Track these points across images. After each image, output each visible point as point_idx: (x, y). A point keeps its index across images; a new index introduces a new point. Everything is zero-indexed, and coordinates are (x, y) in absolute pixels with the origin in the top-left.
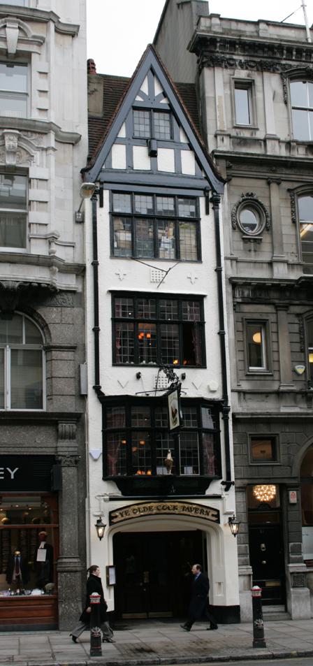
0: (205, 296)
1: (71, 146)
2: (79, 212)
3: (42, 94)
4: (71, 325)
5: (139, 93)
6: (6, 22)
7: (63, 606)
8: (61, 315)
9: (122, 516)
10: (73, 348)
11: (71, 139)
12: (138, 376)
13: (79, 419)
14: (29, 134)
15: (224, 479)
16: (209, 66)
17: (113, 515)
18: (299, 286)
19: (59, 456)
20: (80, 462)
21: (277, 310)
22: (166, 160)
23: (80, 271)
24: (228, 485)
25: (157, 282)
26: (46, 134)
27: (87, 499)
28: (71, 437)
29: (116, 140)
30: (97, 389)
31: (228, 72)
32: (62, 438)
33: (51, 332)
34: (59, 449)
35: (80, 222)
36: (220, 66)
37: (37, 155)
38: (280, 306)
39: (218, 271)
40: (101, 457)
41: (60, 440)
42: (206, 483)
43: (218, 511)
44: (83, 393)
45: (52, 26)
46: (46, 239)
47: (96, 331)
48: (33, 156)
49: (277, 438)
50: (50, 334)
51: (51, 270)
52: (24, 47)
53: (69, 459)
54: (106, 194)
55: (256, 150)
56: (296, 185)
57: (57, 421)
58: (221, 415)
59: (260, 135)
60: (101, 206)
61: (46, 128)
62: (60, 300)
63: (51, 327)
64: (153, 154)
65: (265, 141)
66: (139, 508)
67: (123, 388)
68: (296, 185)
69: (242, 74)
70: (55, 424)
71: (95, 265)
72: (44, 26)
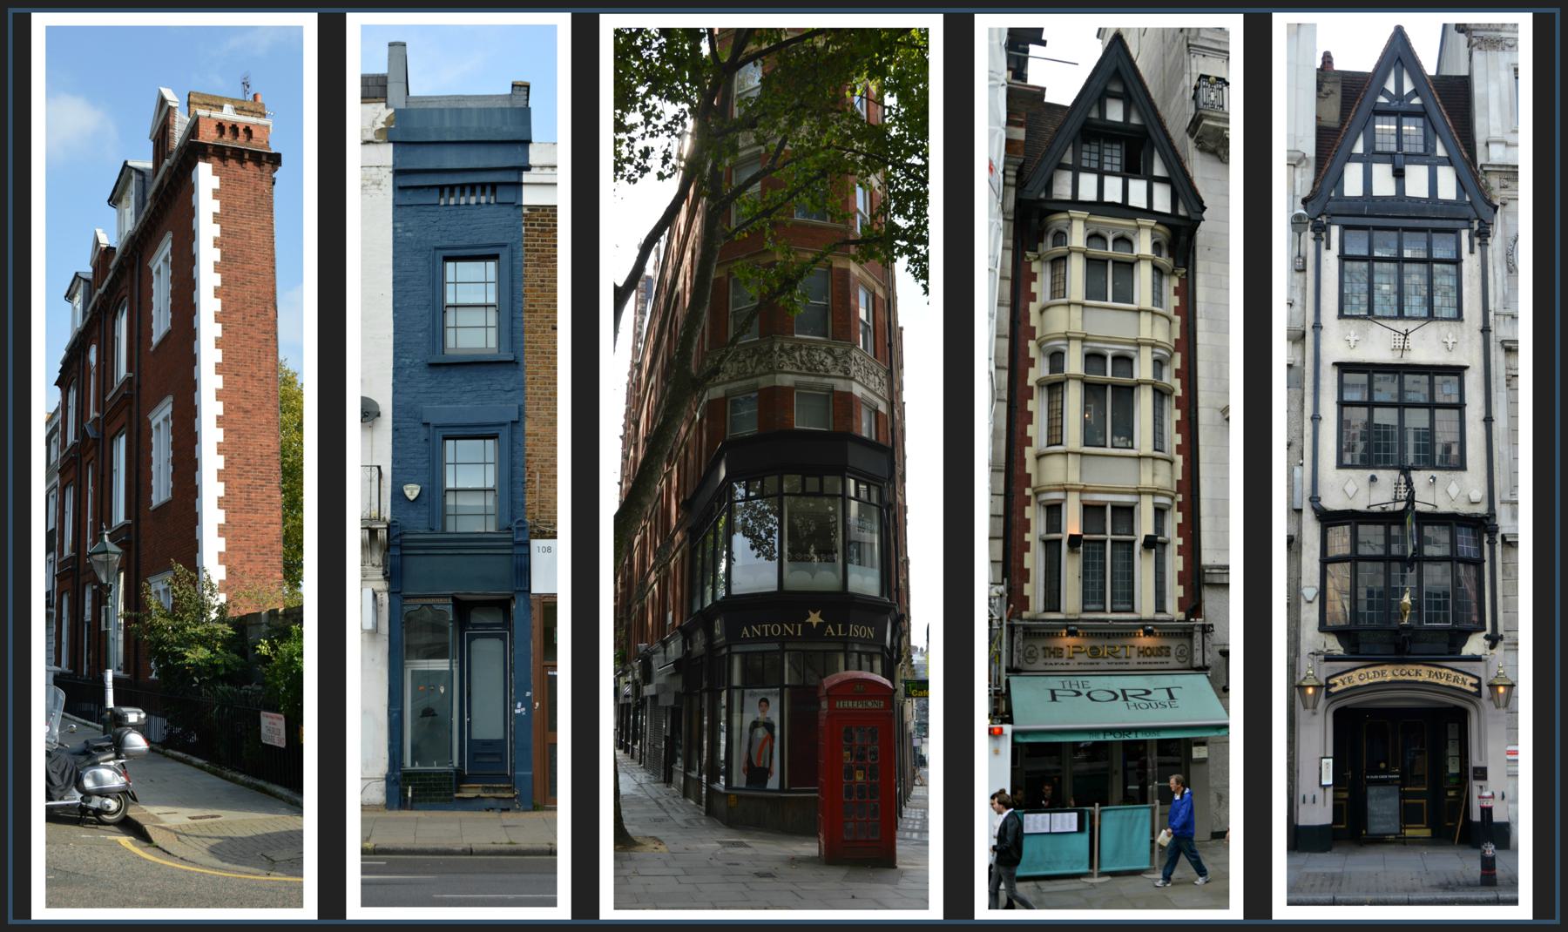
15: (1489, 631)
17: (1331, 682)
30: (1315, 499)
42: (1462, 636)
43: (1479, 679)
58: (1486, 539)
60: (1328, 248)
64: (1399, 174)
71: (1317, 326)
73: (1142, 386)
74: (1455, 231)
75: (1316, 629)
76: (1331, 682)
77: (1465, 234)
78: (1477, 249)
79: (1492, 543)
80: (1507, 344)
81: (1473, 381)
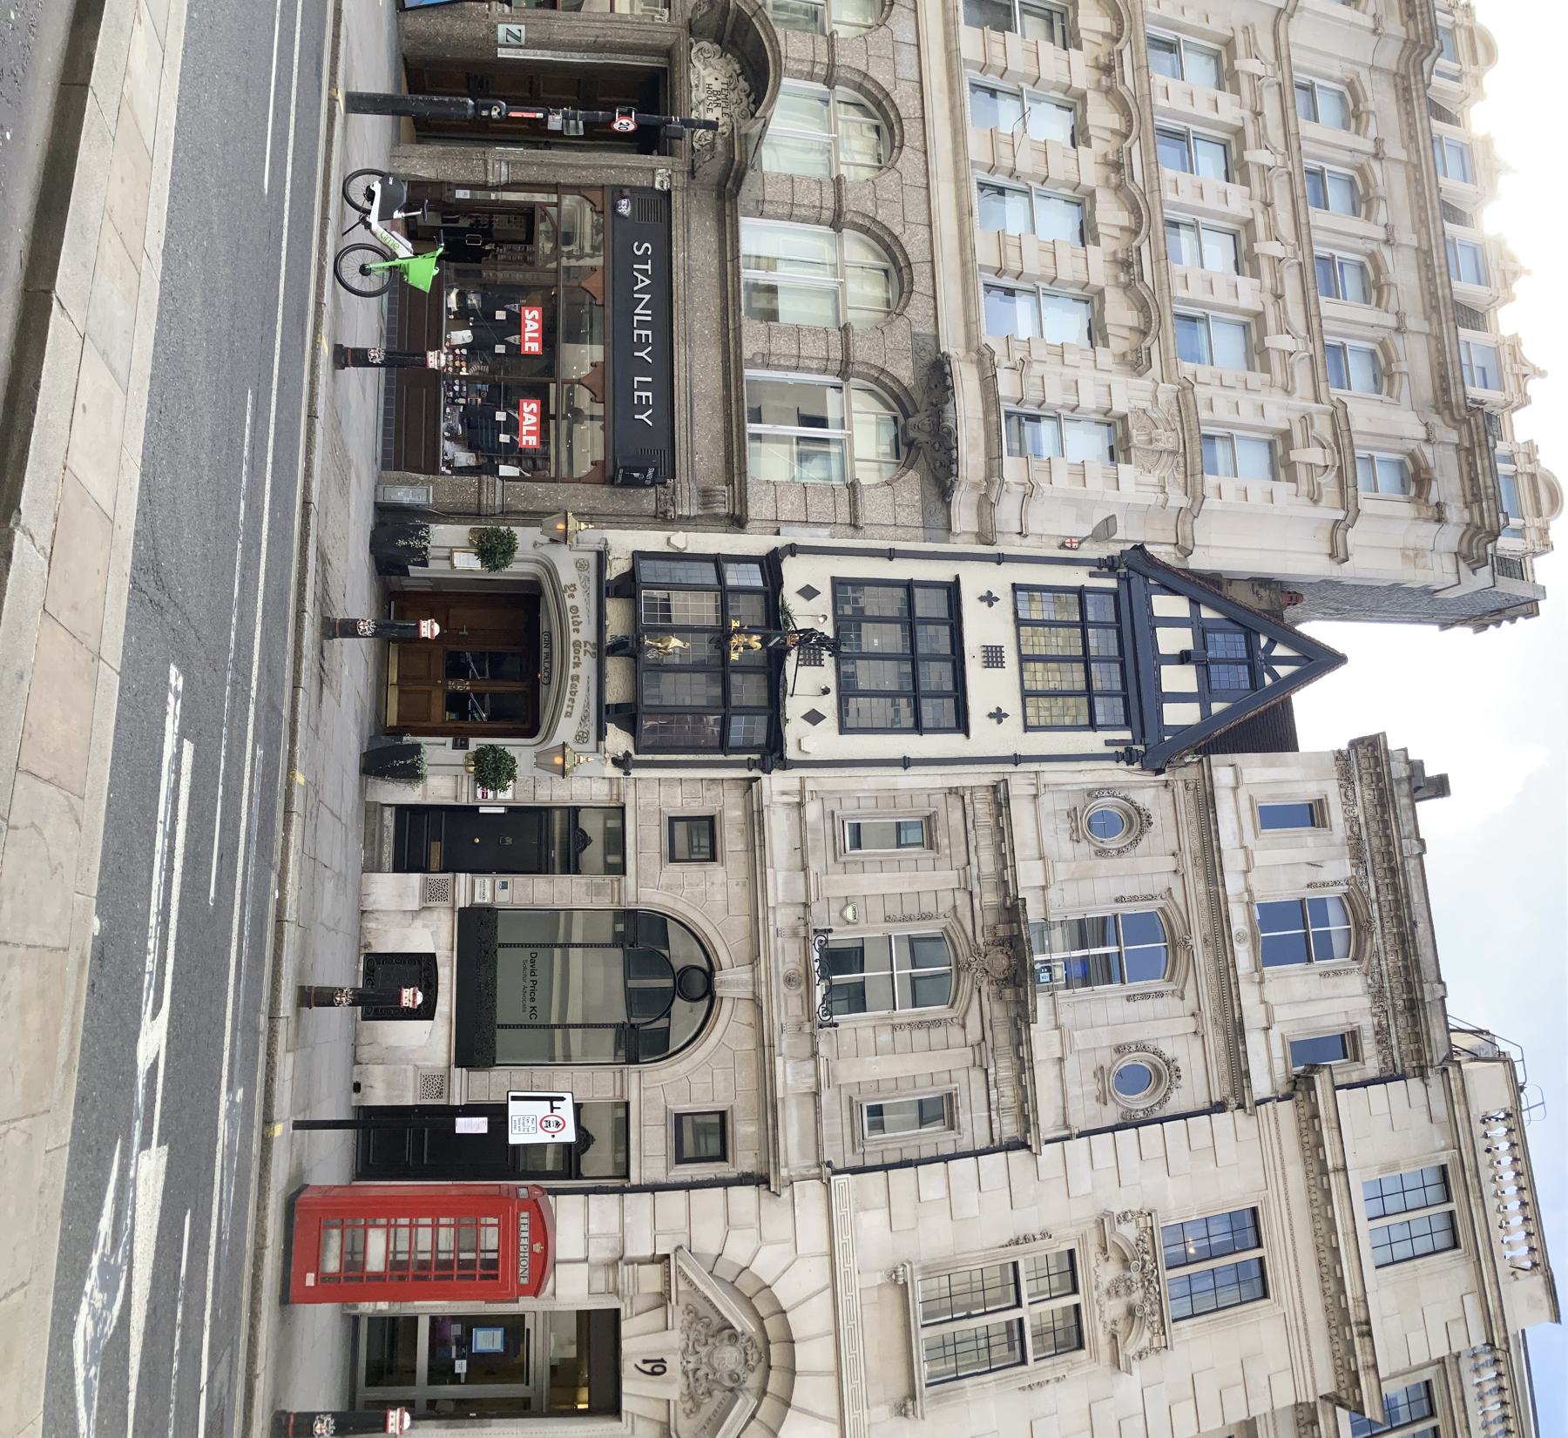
0: (967, 735)
5: (1272, 642)
6: (1332, 448)
13: (738, 522)
20: (662, 519)
22: (1179, 679)
23: (984, 537)
24: (622, 763)
29: (1195, 602)
30: (793, 550)
39: (1016, 760)
40: (671, 550)
45: (1340, 515)
52: (1302, 472)
54: (1111, 583)
56: (1180, 900)
58: (756, 757)
60: (1092, 575)
64: (1184, 658)
68: (1180, 900)
71: (1000, 559)
72: (1339, 506)
74: (1128, 724)
79: (750, 765)
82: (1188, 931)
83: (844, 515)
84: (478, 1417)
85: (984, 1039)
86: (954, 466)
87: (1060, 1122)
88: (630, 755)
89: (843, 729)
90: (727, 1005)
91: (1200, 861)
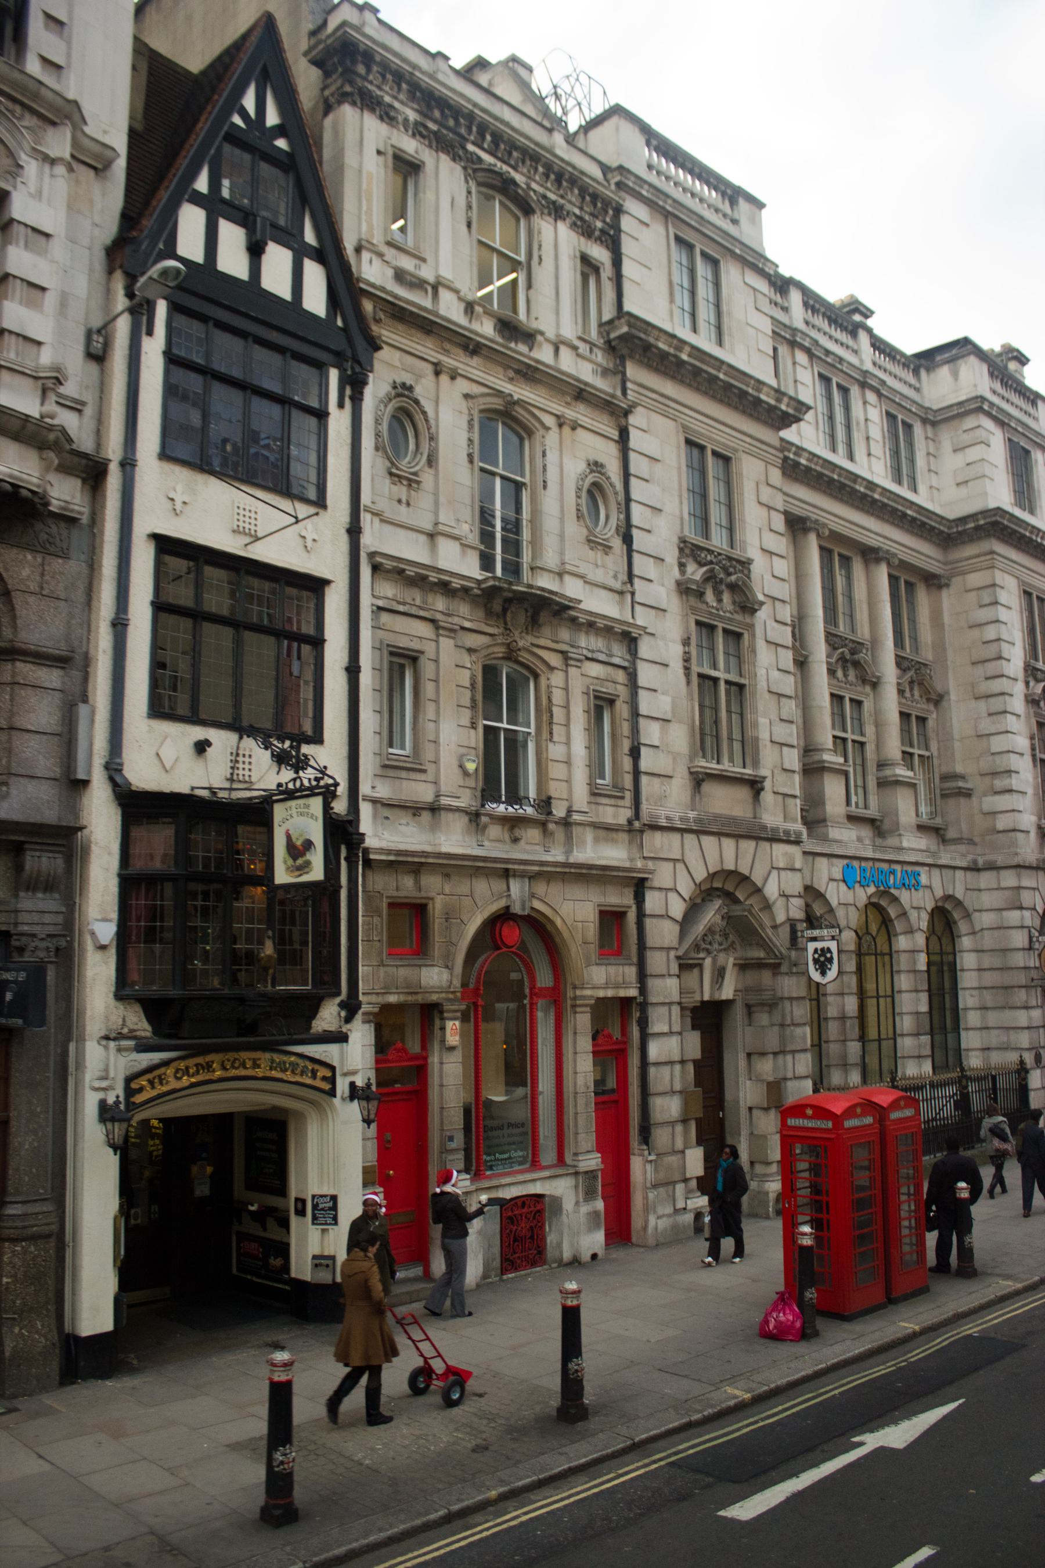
1: (92, 173)
2: (99, 331)
3: (52, 25)
4: (62, 604)
7: (16, 1330)
8: (42, 575)
9: (153, 1087)
10: (60, 661)
11: (97, 157)
12: (201, 747)
14: (18, 109)
16: (354, 104)
17: (134, 1085)
18: (479, 592)
19: (22, 934)
21: (438, 635)
24: (351, 1008)
25: (251, 536)
26: (54, 124)
27: (72, 1046)
28: (48, 886)
30: (113, 769)
31: (383, 128)
32: (28, 889)
33: (18, 613)
34: (24, 917)
35: (98, 357)
36: (373, 110)
37: (31, 167)
38: (444, 628)
40: (115, 943)
41: (22, 894)
42: (311, 1006)
43: (333, 1068)
44: (81, 775)
46: (36, 378)
47: (120, 625)
48: (22, 167)
49: (430, 906)
50: (14, 618)
51: (42, 459)
53: (44, 944)
55: (421, 300)
56: (477, 390)
57: (24, 843)
58: (343, 853)
59: (427, 273)
60: (150, 333)
61: (57, 110)
62: (43, 536)
63: (18, 600)
64: (255, 251)
65: (435, 289)
66: (187, 1068)
67: (167, 771)
68: (477, 390)
69: (410, 145)
70: (17, 850)
71: (128, 464)
73: (442, 813)
74: (320, 367)
75: (111, 995)
76: (134, 1085)
77: (334, 375)
78: (348, 403)
80: (378, 559)
81: (335, 603)
82: (499, 393)
83: (51, 677)
84: (723, 1111)
85: (562, 652)
86: (24, 493)
87: (616, 596)
88: (342, 1001)
89: (317, 738)
90: (537, 905)
91: (448, 346)
